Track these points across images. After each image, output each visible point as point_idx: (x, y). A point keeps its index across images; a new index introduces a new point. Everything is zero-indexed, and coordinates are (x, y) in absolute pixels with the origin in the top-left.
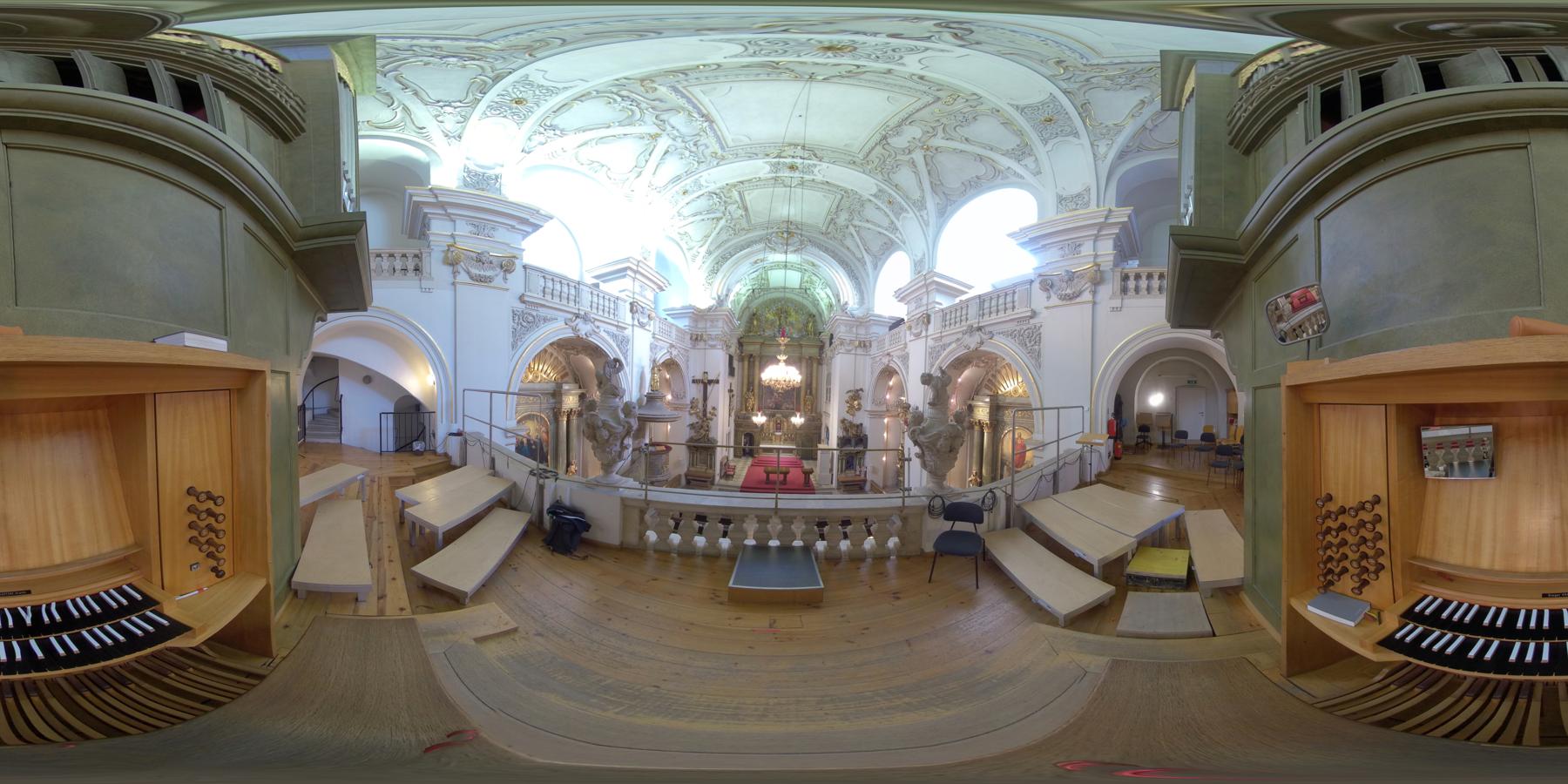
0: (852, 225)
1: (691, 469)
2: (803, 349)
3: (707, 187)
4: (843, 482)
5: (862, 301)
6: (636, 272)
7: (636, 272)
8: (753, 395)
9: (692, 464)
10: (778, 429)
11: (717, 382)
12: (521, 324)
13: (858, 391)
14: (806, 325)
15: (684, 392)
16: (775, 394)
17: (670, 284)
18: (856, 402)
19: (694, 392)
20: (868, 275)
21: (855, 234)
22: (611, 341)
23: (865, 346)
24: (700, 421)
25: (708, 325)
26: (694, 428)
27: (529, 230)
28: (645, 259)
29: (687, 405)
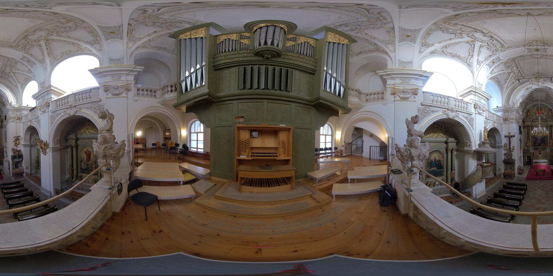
0: (12, 72)
1: (506, 171)
2: (548, 122)
3: (503, 60)
4: (14, 174)
5: (17, 102)
6: (475, 92)
7: (475, 92)
8: (530, 141)
9: (506, 169)
10: (540, 154)
11: (514, 136)
12: (422, 113)
13: (18, 137)
15: (501, 141)
16: (538, 140)
17: (492, 98)
18: (17, 141)
19: (504, 141)
20: (19, 91)
21: (13, 75)
22: (465, 120)
23: (20, 119)
24: (508, 152)
25: (510, 114)
26: (506, 155)
27: (425, 78)
28: (480, 88)
29: (503, 146)
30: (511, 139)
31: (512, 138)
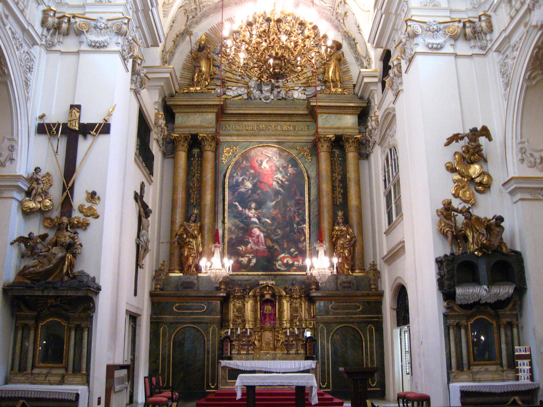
8: (201, 230)
11: (105, 129)
14: (325, 65)
15: (12, 149)
16: (256, 231)
30: (83, 145)
31: (90, 138)
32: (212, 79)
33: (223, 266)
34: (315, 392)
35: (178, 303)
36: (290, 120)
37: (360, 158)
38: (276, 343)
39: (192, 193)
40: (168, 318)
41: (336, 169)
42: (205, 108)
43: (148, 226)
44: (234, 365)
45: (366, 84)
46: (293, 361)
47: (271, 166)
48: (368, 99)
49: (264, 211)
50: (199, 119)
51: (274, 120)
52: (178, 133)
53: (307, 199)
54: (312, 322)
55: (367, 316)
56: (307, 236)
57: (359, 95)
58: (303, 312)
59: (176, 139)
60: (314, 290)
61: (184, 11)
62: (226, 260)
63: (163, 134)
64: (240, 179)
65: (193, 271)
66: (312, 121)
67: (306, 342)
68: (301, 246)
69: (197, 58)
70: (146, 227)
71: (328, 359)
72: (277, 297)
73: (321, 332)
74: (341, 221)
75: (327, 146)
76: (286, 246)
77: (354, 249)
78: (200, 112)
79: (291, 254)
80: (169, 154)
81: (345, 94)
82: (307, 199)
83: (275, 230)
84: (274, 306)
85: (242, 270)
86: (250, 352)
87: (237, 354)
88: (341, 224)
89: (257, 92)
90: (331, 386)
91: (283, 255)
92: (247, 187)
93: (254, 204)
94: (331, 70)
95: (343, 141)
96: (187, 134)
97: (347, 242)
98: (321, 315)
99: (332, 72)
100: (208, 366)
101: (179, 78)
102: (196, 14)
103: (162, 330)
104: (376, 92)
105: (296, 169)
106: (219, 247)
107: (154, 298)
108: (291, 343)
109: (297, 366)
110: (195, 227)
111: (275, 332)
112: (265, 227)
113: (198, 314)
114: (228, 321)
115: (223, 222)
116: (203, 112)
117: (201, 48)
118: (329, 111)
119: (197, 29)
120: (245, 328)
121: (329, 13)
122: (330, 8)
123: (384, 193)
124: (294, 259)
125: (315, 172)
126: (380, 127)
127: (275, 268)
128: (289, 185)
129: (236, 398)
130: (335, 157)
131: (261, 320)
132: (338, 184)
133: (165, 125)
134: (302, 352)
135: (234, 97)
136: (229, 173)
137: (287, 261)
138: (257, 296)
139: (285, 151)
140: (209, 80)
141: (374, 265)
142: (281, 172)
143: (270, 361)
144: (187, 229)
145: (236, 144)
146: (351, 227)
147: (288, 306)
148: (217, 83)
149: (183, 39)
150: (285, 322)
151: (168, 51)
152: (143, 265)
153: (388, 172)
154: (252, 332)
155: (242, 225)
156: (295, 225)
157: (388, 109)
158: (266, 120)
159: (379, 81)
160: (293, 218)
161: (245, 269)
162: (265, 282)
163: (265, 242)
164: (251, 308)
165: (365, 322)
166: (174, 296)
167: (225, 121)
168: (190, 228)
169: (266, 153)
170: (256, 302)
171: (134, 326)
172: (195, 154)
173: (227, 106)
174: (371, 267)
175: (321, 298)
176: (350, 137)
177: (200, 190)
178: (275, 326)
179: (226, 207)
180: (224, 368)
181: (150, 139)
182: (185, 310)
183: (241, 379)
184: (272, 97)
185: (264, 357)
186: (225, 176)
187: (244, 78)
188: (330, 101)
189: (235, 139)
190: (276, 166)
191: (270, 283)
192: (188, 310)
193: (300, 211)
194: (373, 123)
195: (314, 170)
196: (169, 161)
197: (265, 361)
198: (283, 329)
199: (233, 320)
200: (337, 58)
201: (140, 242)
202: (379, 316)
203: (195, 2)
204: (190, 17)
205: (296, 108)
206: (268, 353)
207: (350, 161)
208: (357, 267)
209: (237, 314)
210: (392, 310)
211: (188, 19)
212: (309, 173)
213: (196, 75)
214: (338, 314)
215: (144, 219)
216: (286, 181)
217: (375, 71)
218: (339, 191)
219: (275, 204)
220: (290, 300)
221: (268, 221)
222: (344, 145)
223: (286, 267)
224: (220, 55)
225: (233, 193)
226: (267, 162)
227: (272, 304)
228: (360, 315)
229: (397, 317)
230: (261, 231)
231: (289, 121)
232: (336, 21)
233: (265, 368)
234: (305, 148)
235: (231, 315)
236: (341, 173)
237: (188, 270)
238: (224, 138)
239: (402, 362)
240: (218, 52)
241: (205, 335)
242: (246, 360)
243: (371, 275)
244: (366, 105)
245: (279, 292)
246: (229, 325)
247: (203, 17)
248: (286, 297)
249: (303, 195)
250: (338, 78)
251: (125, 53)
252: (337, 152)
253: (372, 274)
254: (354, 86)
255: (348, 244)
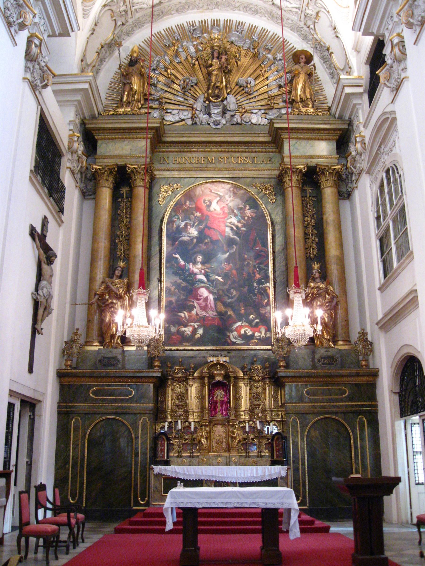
16: (204, 292)
32: (146, 100)
33: (149, 321)
34: (294, 518)
35: (96, 386)
36: (247, 150)
37: (340, 197)
38: (230, 442)
39: (119, 243)
40: (82, 406)
41: (308, 212)
42: (136, 132)
43: (51, 276)
44: (172, 472)
45: (348, 95)
46: (254, 467)
47: (223, 207)
48: (350, 118)
49: (214, 265)
50: (128, 147)
51: (227, 150)
52: (100, 164)
53: (270, 250)
54: (280, 413)
55: (356, 403)
56: (272, 297)
57: (337, 115)
58: (268, 399)
59: (98, 173)
60: (282, 368)
61: (110, 12)
62: (153, 312)
63: (80, 165)
64: (182, 224)
65: (117, 343)
66: (275, 152)
67: (272, 440)
68: (264, 312)
69: (127, 74)
70: (48, 277)
71: (303, 464)
72: (232, 379)
73: (293, 426)
74: (317, 275)
75: (297, 180)
76: (243, 312)
77: (336, 314)
78: (129, 138)
79: (250, 322)
80: (90, 193)
81: (318, 115)
82: (270, 250)
83: (228, 290)
84: (227, 392)
85: (185, 344)
86: (195, 454)
87: (177, 456)
88: (318, 280)
89: (205, 116)
90: (308, 501)
91: (239, 323)
92: (191, 235)
93: (201, 257)
94: (300, 86)
95: (317, 174)
96: (112, 165)
97: (327, 303)
98: (293, 403)
99: (301, 89)
100: (136, 474)
101: (104, 100)
102: (127, 21)
103: (74, 424)
104: (361, 107)
105: (256, 211)
106: (145, 295)
107: (63, 379)
108: (251, 441)
109: (260, 474)
110: (120, 284)
111: (229, 427)
112: (215, 287)
113: (122, 401)
114: (164, 411)
115: (160, 281)
116: (133, 138)
117: (133, 62)
118: (299, 136)
119: (128, 42)
120: (188, 422)
121: (296, 18)
122: (297, 10)
123: (377, 235)
124: (255, 329)
125: (281, 216)
126: (368, 152)
127: (229, 340)
128: (246, 232)
129: (164, 529)
130: (306, 196)
131: (210, 410)
132: (312, 231)
133: (83, 153)
134: (267, 454)
135: (174, 123)
136: (168, 216)
137: (245, 331)
138: (204, 378)
139: (241, 188)
140: (142, 102)
141: (363, 334)
142: (236, 215)
143: (222, 467)
144: (110, 287)
145: (178, 180)
146: (330, 283)
147: (246, 391)
148: (153, 105)
149: (110, 54)
150: (242, 413)
151: (91, 64)
152: (42, 329)
153: (384, 205)
154: (197, 426)
155: (184, 284)
156: (255, 284)
157: (384, 114)
158: (216, 150)
159: (365, 91)
160: (253, 275)
161: (189, 343)
162: (215, 359)
163: (216, 305)
164: (196, 394)
165: (353, 412)
166: (90, 377)
167: (163, 152)
168: (113, 285)
169: (217, 191)
170: (202, 385)
171: (32, 417)
172: (123, 193)
173: (166, 132)
174: (360, 337)
175: (294, 378)
176: (327, 168)
177: (128, 240)
178: (229, 418)
179: (164, 261)
180: (158, 476)
181: (61, 167)
182: (105, 396)
183: (173, 497)
184: (223, 121)
185: (215, 461)
186: (162, 221)
187: (187, 100)
188: (300, 121)
189: (176, 174)
190: (229, 208)
191: (223, 359)
192: (110, 395)
193: (262, 266)
194: (359, 146)
195: (280, 213)
196: (89, 204)
197: (215, 467)
198: (240, 422)
199: (172, 411)
200: (307, 72)
201: (38, 297)
202: (373, 403)
203: (125, 2)
204: (119, 23)
205: (254, 133)
206: (220, 456)
207: (327, 200)
208: (340, 338)
209: (177, 402)
210: (393, 395)
211: (116, 25)
212: (273, 217)
213: (126, 93)
214: (316, 401)
215: (45, 267)
216: (243, 226)
217: (360, 78)
218: (314, 240)
219: (228, 256)
220: (250, 382)
221: (220, 278)
222: (318, 180)
223: (243, 339)
224: (157, 72)
225: (173, 244)
226: (217, 202)
227: (225, 389)
228: (345, 402)
229: (400, 404)
230: (210, 292)
231: (245, 152)
232: (305, 28)
233: (215, 476)
234: (268, 186)
235: (169, 404)
236: (315, 216)
237: (110, 341)
238: (161, 173)
239: (408, 467)
240: (155, 67)
241: (132, 430)
242: (190, 465)
243: (360, 347)
244: (347, 127)
245: (235, 372)
246: (166, 418)
247: (136, 26)
248: (244, 379)
249: (265, 245)
250: (308, 96)
251: (9, 12)
252: (309, 190)
253: (361, 346)
254: (329, 108)
255: (328, 306)
